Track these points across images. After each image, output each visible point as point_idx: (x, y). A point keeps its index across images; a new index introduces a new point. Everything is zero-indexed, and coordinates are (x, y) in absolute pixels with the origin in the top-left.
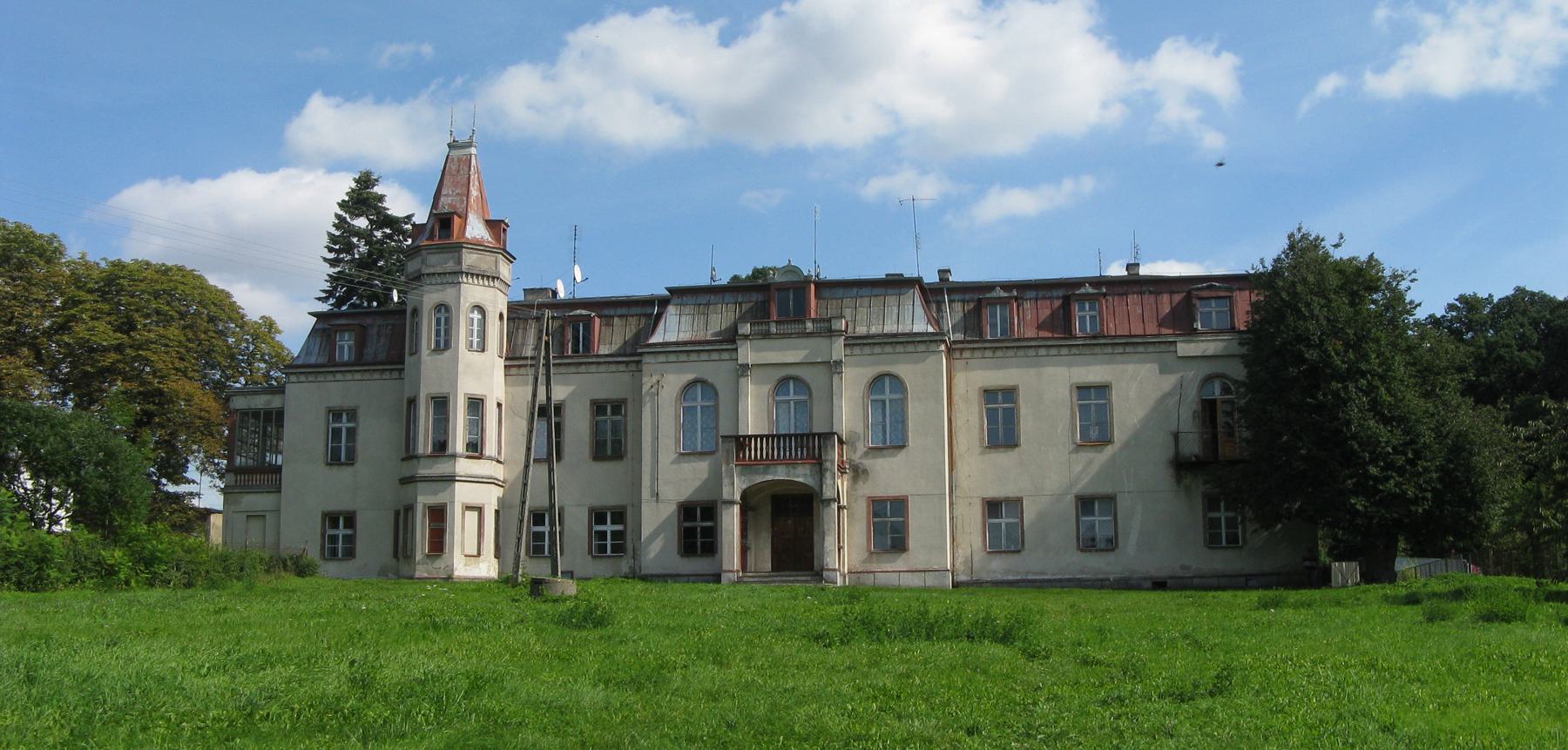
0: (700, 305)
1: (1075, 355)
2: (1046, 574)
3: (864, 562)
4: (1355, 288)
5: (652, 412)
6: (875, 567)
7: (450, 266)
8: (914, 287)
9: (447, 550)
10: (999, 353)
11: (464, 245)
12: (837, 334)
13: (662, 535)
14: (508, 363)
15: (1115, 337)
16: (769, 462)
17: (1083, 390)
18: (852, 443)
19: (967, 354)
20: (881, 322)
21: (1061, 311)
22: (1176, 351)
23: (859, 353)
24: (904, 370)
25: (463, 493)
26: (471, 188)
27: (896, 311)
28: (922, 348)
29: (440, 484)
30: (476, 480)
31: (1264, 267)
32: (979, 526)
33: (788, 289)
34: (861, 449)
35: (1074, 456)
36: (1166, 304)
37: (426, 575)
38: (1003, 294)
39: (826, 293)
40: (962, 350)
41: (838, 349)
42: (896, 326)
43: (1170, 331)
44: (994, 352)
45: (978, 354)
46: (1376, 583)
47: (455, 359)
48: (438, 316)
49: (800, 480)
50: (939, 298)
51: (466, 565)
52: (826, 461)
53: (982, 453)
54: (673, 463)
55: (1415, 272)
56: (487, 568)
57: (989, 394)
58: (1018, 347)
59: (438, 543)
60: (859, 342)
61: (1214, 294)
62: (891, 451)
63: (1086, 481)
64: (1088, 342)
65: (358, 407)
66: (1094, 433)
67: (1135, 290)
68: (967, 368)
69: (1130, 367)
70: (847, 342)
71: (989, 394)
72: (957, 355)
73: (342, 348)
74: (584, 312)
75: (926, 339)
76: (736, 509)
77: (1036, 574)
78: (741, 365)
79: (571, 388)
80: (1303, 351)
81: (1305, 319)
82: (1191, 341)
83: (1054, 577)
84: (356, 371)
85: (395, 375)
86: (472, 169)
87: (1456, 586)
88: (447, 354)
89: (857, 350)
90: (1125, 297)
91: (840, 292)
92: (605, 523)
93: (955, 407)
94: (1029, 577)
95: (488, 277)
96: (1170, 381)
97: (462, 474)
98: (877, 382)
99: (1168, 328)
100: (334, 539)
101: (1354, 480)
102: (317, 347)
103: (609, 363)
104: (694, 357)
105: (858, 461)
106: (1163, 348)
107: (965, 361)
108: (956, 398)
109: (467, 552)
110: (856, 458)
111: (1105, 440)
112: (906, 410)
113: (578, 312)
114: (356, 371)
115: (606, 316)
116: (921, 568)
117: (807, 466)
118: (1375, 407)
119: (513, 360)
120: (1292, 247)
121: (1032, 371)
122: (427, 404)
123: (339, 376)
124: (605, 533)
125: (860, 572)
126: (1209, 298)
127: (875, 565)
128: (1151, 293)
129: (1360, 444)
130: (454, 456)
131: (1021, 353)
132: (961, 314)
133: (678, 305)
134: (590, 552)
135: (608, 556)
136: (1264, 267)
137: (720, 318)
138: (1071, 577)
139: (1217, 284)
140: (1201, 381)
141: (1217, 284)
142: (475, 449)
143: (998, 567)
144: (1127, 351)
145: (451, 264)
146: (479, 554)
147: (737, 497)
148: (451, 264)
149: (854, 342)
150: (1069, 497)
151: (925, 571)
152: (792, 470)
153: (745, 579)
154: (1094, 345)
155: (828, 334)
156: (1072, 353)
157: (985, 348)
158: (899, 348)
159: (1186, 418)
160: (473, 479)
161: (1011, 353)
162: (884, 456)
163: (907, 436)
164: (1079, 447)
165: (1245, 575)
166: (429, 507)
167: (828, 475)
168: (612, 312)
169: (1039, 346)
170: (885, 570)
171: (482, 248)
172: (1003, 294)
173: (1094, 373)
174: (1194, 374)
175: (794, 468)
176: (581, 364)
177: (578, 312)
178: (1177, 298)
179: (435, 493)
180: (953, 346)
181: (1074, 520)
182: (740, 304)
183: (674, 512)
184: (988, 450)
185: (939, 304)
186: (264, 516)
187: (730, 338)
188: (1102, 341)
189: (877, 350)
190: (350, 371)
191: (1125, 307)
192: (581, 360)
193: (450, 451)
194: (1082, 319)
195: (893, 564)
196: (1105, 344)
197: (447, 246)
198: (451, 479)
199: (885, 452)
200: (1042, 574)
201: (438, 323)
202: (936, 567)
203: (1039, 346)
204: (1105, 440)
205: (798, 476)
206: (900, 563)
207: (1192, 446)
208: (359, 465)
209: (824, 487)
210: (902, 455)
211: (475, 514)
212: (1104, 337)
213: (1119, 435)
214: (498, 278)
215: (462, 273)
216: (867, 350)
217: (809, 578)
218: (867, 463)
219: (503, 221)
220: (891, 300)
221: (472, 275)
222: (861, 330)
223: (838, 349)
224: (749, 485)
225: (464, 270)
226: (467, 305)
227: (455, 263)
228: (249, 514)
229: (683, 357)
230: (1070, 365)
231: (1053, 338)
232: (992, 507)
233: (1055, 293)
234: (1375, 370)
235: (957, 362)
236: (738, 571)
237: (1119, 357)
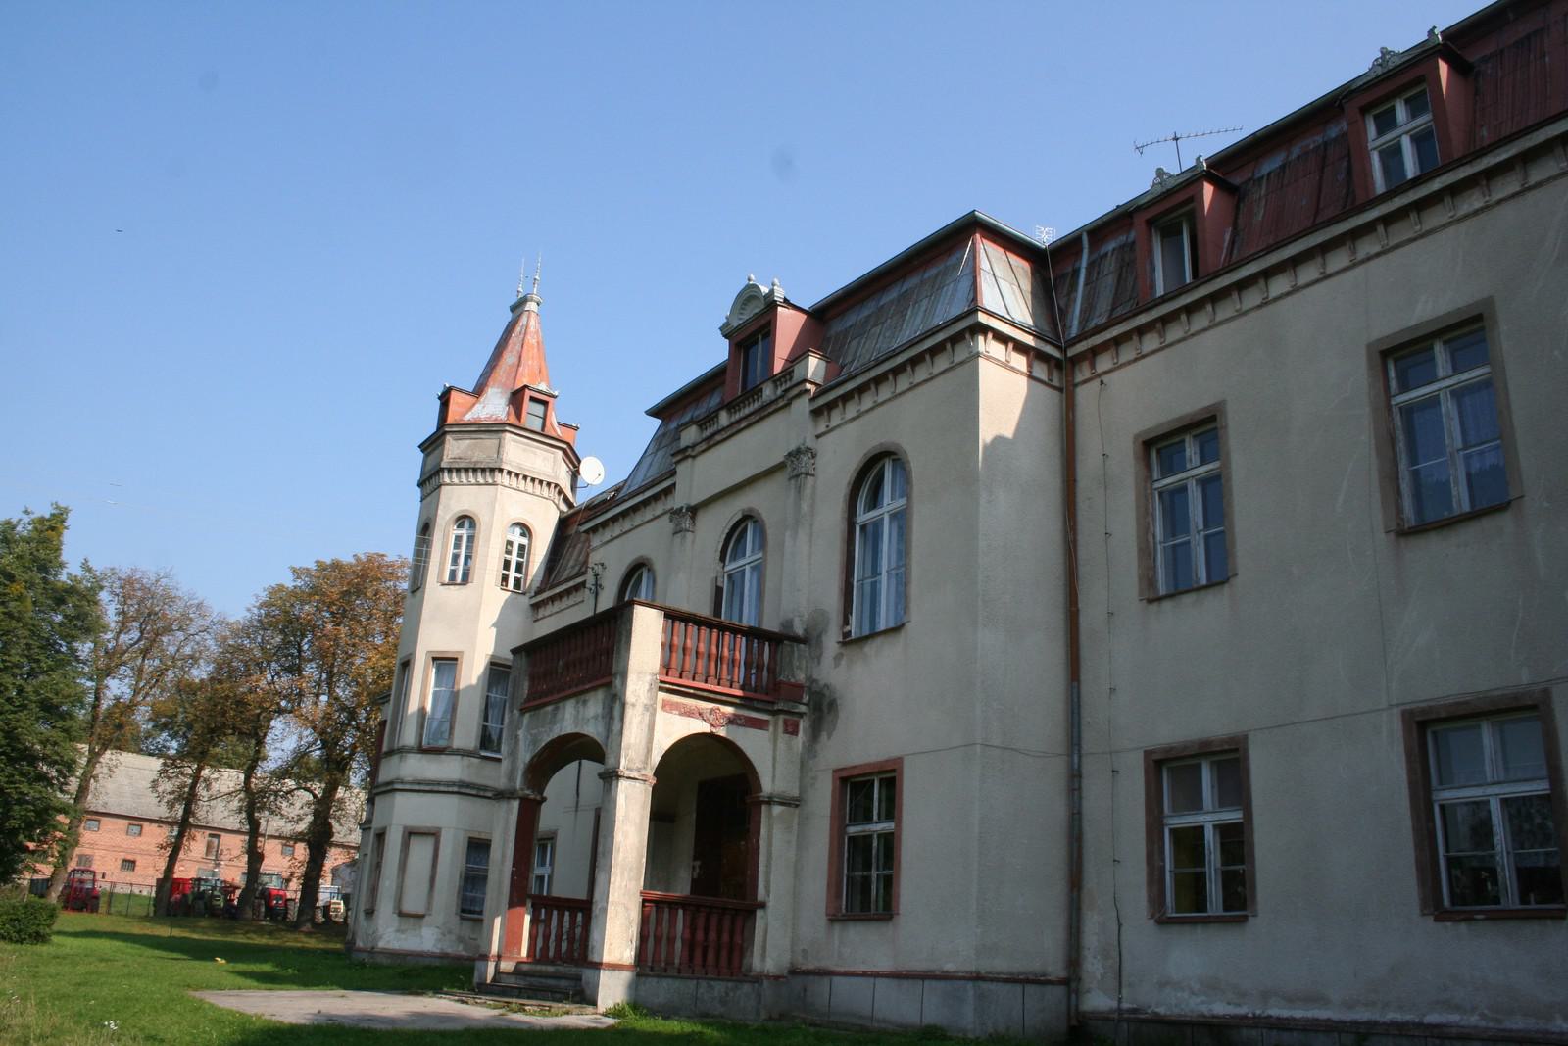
1: (1369, 258)
10: (1174, 332)
19: (1104, 363)
44: (1162, 335)
46: (1445, 704)
51: (398, 931)
72: (1083, 373)
77: (1290, 1000)
87: (336, 835)
94: (1277, 1010)
95: (483, 470)
107: (1098, 380)
131: (1225, 310)
138: (1408, 1017)
180: (1071, 352)
219: (526, 387)
221: (458, 470)
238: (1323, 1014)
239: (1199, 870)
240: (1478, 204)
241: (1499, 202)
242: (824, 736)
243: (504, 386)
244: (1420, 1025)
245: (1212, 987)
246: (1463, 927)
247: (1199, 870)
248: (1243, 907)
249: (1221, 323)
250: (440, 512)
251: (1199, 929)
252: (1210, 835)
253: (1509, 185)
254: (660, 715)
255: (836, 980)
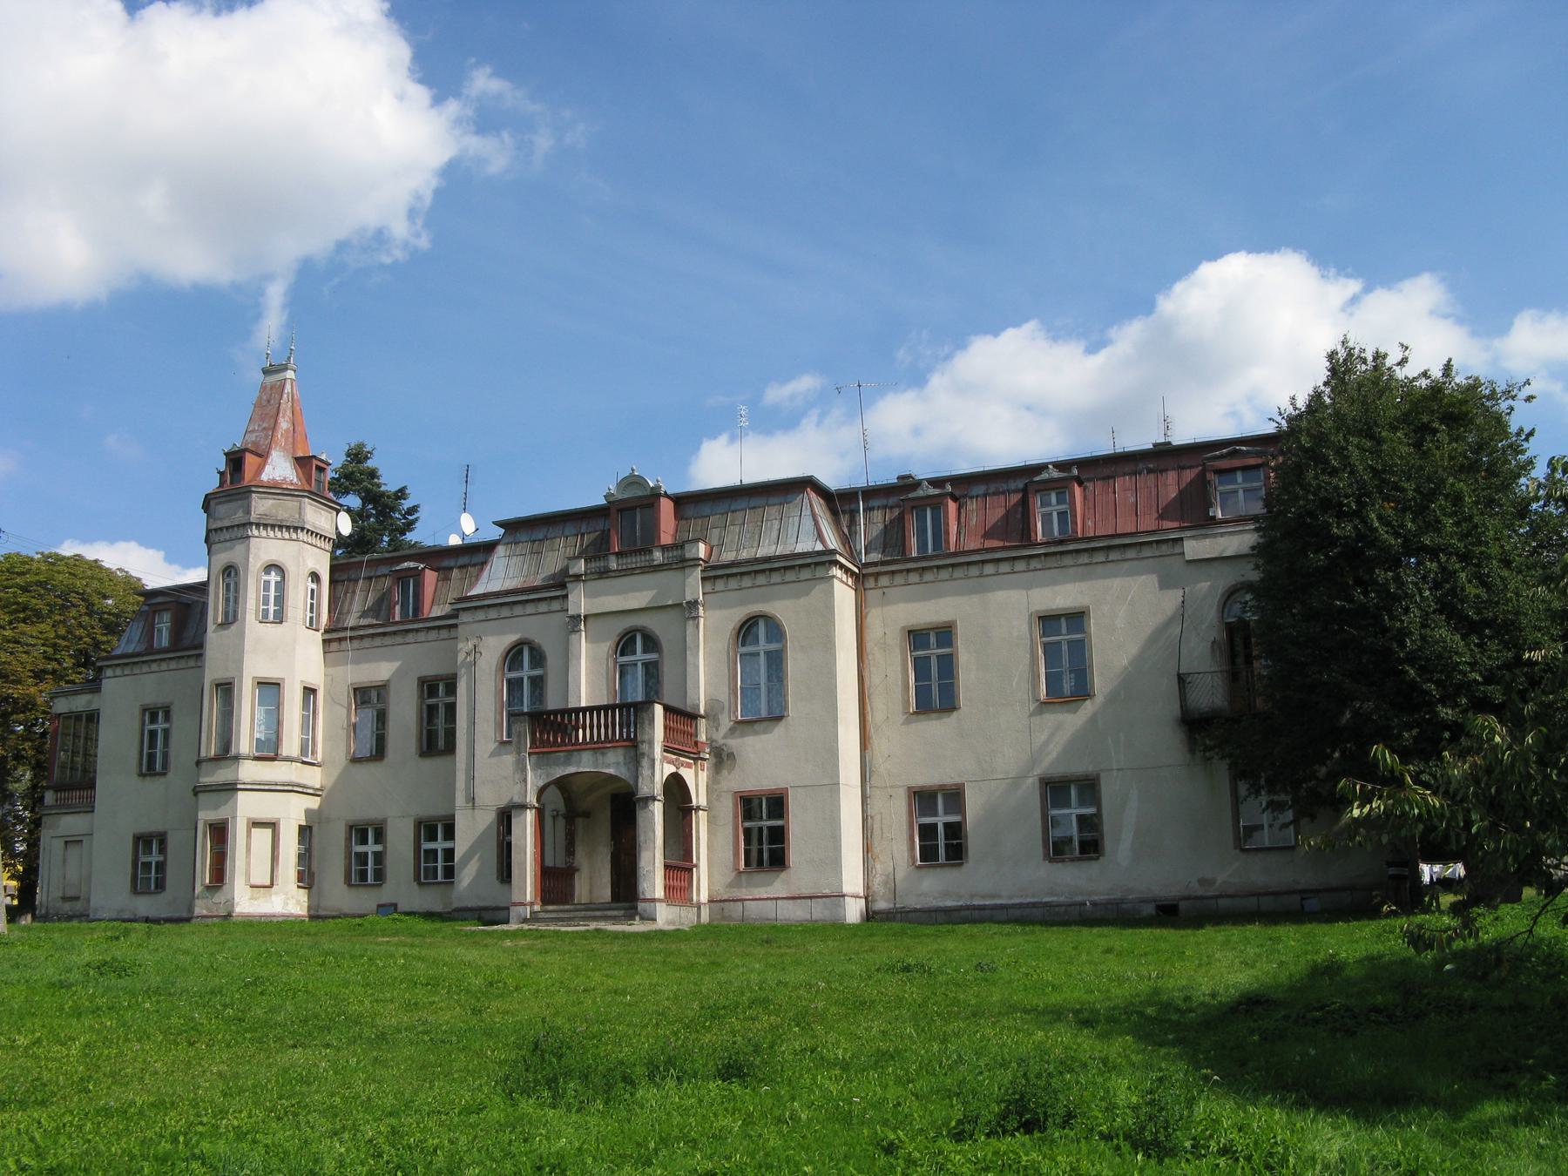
0: (535, 541)
1: (1036, 570)
2: (999, 896)
3: (730, 886)
4: (1425, 419)
5: (468, 684)
6: (743, 893)
7: (239, 517)
8: (805, 489)
9: (227, 880)
10: (928, 576)
11: (254, 489)
12: (692, 563)
13: (476, 857)
14: (327, 636)
15: (1091, 539)
16: (600, 745)
17: (1048, 621)
18: (711, 716)
19: (884, 581)
20: (756, 544)
21: (1020, 509)
22: (1184, 553)
23: (723, 589)
24: (784, 609)
25: (247, 806)
26: (281, 420)
27: (776, 527)
28: (806, 574)
29: (223, 794)
30: (267, 787)
31: (1295, 409)
32: (905, 827)
33: (633, 509)
34: (726, 723)
35: (1036, 720)
36: (1171, 485)
37: (205, 912)
38: (933, 491)
39: (690, 510)
40: (877, 575)
41: (694, 586)
42: (774, 547)
43: (1176, 525)
45: (899, 579)
47: (241, 635)
48: (227, 580)
49: (611, 771)
50: (853, 506)
51: (252, 898)
52: (643, 742)
53: (907, 722)
54: (492, 755)
55: (1528, 382)
56: (289, 901)
57: (916, 637)
58: (953, 566)
59: (219, 875)
60: (720, 572)
61: (1236, 463)
62: (764, 724)
63: (1054, 754)
64: (1053, 549)
65: (172, 703)
66: (1067, 685)
67: (1127, 469)
68: (885, 601)
69: (1116, 583)
70: (706, 574)
71: (916, 637)
72: (870, 583)
73: (160, 631)
74: (412, 564)
75: (809, 561)
76: (530, 816)
77: (983, 897)
78: (572, 617)
79: (396, 665)
80: (1330, 524)
81: (1334, 472)
82: (1206, 536)
83: (1012, 902)
84: (170, 659)
85: (192, 663)
86: (285, 396)
88: (233, 627)
89: (720, 585)
90: (1111, 481)
91: (706, 508)
92: (947, 825)
93: (869, 659)
94: (976, 902)
95: (288, 528)
96: (1170, 601)
97: (246, 781)
98: (746, 630)
99: (1172, 521)
100: (362, 859)
101: (1415, 732)
102: (139, 633)
103: (439, 628)
104: (518, 610)
105: (721, 742)
106: (1164, 549)
108: (870, 645)
109: (254, 881)
110: (719, 736)
111: (1082, 692)
112: (690, 658)
113: (406, 565)
114: (170, 659)
115: (444, 569)
116: (806, 892)
117: (620, 752)
118: (1450, 608)
119: (335, 637)
120: (1333, 371)
121: (975, 599)
122: (211, 689)
123: (154, 667)
124: (435, 851)
125: (725, 901)
126: (1233, 470)
127: (744, 890)
128: (1150, 471)
129: (1422, 670)
130: (237, 758)
131: (959, 573)
132: (881, 526)
133: (508, 544)
134: (417, 878)
135: (440, 883)
136: (1295, 409)
137: (556, 555)
139: (1244, 448)
140: (1223, 595)
141: (1244, 448)
142: (269, 752)
143: (936, 887)
144: (1111, 558)
145: (240, 514)
146: (272, 885)
147: (531, 798)
148: (240, 514)
149: (716, 573)
150: (1030, 780)
151: (811, 898)
152: (600, 757)
153: (542, 915)
154: (1062, 553)
155: (680, 565)
156: (1032, 567)
157: (908, 571)
158: (776, 577)
159: (1200, 654)
160: (262, 787)
161: (944, 574)
162: (756, 733)
163: (786, 702)
164: (1044, 706)
165: (1301, 892)
166: (210, 825)
167: (645, 762)
168: (452, 563)
169: (984, 562)
170: (757, 897)
171: (278, 491)
172: (933, 491)
173: (1062, 595)
174: (1207, 588)
175: (603, 754)
176: (407, 631)
177: (406, 565)
178: (1189, 475)
179: (216, 807)
180: (864, 571)
181: (1038, 815)
182: (583, 535)
183: (489, 827)
184: (914, 717)
185: (853, 514)
186: (81, 841)
187: (560, 583)
188: (1071, 547)
189: (747, 582)
190: (155, 661)
191: (1111, 495)
192: (411, 627)
193: (233, 752)
194: (1047, 519)
195: (769, 889)
196: (1078, 551)
197: (234, 492)
198: (231, 788)
199: (756, 726)
200: (993, 896)
201: (228, 586)
202: (827, 891)
203: (984, 562)
204: (1082, 692)
205: (608, 766)
206: (778, 885)
207: (1210, 694)
208: (170, 775)
209: (640, 780)
210: (779, 730)
211: (269, 832)
212: (1076, 540)
213: (1101, 683)
214: (303, 529)
215: (251, 524)
216: (733, 583)
217: (621, 913)
218: (733, 743)
219: (314, 457)
220: (773, 511)
222: (728, 556)
223: (694, 586)
224: (546, 781)
225: (252, 520)
226: (259, 565)
227: (243, 512)
228: (67, 839)
229: (505, 612)
230: (1028, 587)
231: (1004, 548)
232: (923, 799)
233: (1013, 485)
234: (1451, 545)
235: (870, 593)
236: (532, 904)
237: (1099, 569)
238: (999, 902)
239: (779, 823)
240: (1087, 561)
241: (1097, 563)
242: (725, 772)
243: (284, 449)
244: (1041, 903)
245: (945, 894)
246: (1060, 864)
247: (779, 823)
248: (961, 859)
249: (955, 579)
250: (251, 559)
251: (938, 870)
252: (941, 828)
253: (1100, 557)
254: (665, 764)
255: (746, 903)
